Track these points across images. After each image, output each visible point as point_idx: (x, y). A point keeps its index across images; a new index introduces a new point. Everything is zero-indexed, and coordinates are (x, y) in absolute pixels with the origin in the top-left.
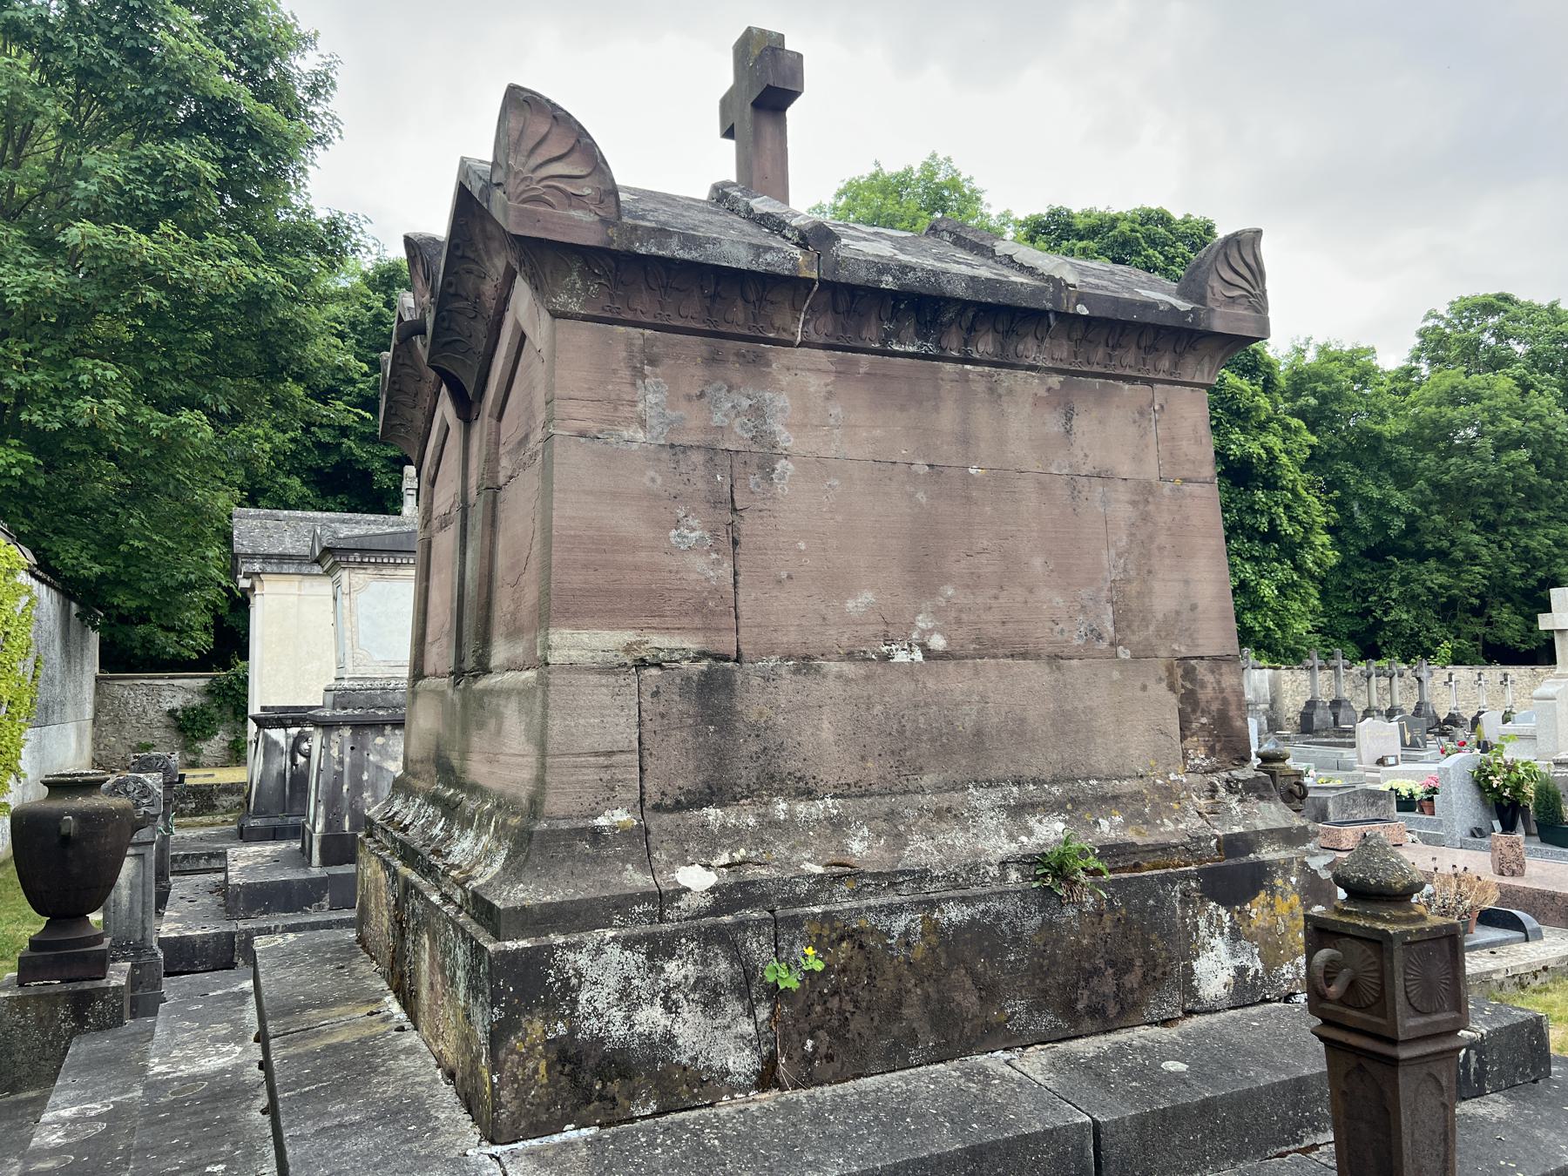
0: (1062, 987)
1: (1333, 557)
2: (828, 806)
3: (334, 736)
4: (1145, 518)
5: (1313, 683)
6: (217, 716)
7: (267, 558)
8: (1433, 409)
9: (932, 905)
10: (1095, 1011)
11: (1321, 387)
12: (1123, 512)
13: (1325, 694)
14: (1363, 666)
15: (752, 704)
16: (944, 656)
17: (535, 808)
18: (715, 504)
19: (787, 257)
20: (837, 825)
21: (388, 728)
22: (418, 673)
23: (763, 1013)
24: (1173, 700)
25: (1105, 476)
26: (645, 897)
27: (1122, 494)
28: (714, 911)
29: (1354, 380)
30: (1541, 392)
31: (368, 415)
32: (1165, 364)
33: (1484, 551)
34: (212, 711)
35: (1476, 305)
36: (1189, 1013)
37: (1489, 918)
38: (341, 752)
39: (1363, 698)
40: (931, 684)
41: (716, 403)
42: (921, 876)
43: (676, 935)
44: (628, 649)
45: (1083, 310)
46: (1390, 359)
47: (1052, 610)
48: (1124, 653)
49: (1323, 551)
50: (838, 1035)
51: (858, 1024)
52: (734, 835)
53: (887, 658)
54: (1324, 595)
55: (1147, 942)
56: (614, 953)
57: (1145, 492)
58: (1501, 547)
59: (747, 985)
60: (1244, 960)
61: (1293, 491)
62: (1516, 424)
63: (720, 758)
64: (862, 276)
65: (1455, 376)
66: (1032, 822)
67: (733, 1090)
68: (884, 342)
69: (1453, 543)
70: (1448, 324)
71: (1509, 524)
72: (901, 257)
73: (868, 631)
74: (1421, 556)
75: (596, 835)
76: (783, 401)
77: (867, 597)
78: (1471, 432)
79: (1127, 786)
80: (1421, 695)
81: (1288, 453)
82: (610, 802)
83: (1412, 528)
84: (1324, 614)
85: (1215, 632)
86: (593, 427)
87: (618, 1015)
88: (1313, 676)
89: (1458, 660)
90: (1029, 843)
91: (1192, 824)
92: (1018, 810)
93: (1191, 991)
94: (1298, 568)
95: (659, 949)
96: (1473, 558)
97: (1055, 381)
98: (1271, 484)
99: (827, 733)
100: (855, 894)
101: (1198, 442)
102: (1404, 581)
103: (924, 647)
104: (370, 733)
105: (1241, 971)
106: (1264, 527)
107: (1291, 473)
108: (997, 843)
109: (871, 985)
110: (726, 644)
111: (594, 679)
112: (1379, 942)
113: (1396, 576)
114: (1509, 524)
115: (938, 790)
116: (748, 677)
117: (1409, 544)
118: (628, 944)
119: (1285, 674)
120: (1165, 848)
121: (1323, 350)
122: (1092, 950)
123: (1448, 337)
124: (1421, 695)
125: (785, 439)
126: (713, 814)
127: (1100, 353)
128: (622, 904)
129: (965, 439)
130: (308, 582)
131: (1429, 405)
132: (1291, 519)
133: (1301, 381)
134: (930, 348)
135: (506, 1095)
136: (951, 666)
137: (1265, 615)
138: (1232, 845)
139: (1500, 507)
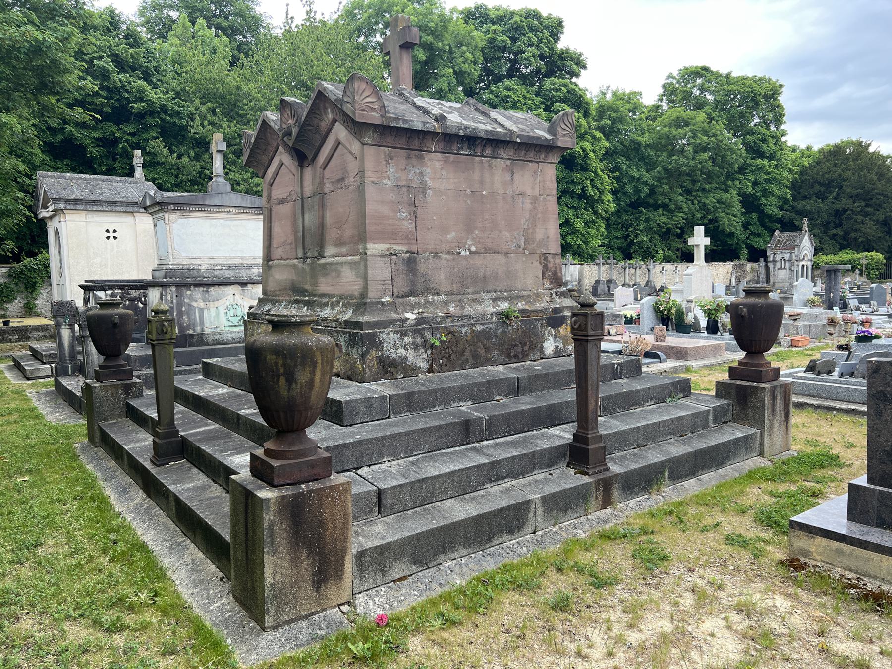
0: (507, 349)
1: (613, 207)
2: (443, 297)
3: (168, 290)
4: (535, 208)
5: (599, 272)
6: (15, 289)
7: (67, 201)
8: (667, 129)
9: (473, 325)
10: (516, 356)
11: (613, 115)
12: (528, 206)
13: (604, 277)
14: (623, 263)
15: (422, 267)
16: (475, 253)
17: (363, 295)
18: (410, 205)
19: (433, 126)
20: (446, 303)
21: (192, 287)
22: (268, 257)
23: (429, 352)
24: (540, 267)
25: (523, 194)
26: (398, 320)
27: (528, 200)
28: (415, 325)
29: (630, 111)
30: (717, 121)
31: (98, 117)
32: (543, 156)
33: (685, 205)
34: (13, 286)
35: (692, 72)
36: (542, 358)
37: (647, 355)
38: (172, 298)
39: (622, 279)
40: (471, 262)
41: (409, 172)
42: (470, 317)
43: (407, 330)
44: (388, 250)
45: (518, 140)
46: (649, 99)
47: (507, 238)
48: (527, 252)
49: (609, 204)
50: (448, 359)
51: (453, 356)
52: (418, 305)
53: (459, 253)
54: (608, 227)
55: (530, 338)
56: (392, 334)
57: (535, 199)
58: (693, 203)
59: (426, 345)
60: (558, 344)
61: (595, 173)
62: (705, 138)
63: (413, 283)
64: (454, 131)
65: (680, 112)
66: (499, 303)
67: (422, 372)
68: (458, 150)
69: (671, 200)
70: (678, 82)
71: (698, 190)
72: (464, 122)
73: (453, 245)
74: (656, 207)
75: (382, 303)
76: (428, 170)
77: (453, 234)
78: (684, 141)
79: (526, 293)
80: (649, 277)
81: (594, 151)
82: (385, 295)
83: (652, 192)
84: (607, 237)
85: (555, 246)
86: (375, 180)
87: (393, 351)
88: (599, 269)
89: (667, 259)
90: (499, 309)
91: (545, 304)
92: (495, 300)
93: (543, 352)
94: (595, 213)
95: (403, 334)
96: (679, 208)
97: (509, 162)
98: (584, 169)
99: (442, 276)
100: (452, 321)
101: (552, 182)
102: (647, 220)
103: (469, 250)
104: (184, 290)
105: (557, 347)
106: (579, 192)
107: (595, 163)
108: (490, 309)
109: (456, 346)
110: (414, 249)
111: (379, 258)
112: (585, 315)
113: (643, 218)
114: (698, 190)
115: (473, 294)
116: (420, 258)
117: (651, 201)
118: (395, 332)
119: (586, 267)
120: (537, 311)
121: (615, 94)
122: (515, 339)
123: (677, 89)
124: (649, 277)
125: (430, 183)
126: (412, 299)
127: (523, 153)
128: (393, 321)
129: (482, 182)
130: (90, 215)
131: (665, 127)
132: (593, 187)
133: (603, 110)
134: (472, 152)
135: (367, 370)
136: (477, 256)
137: (577, 237)
138: (556, 311)
139: (694, 182)
